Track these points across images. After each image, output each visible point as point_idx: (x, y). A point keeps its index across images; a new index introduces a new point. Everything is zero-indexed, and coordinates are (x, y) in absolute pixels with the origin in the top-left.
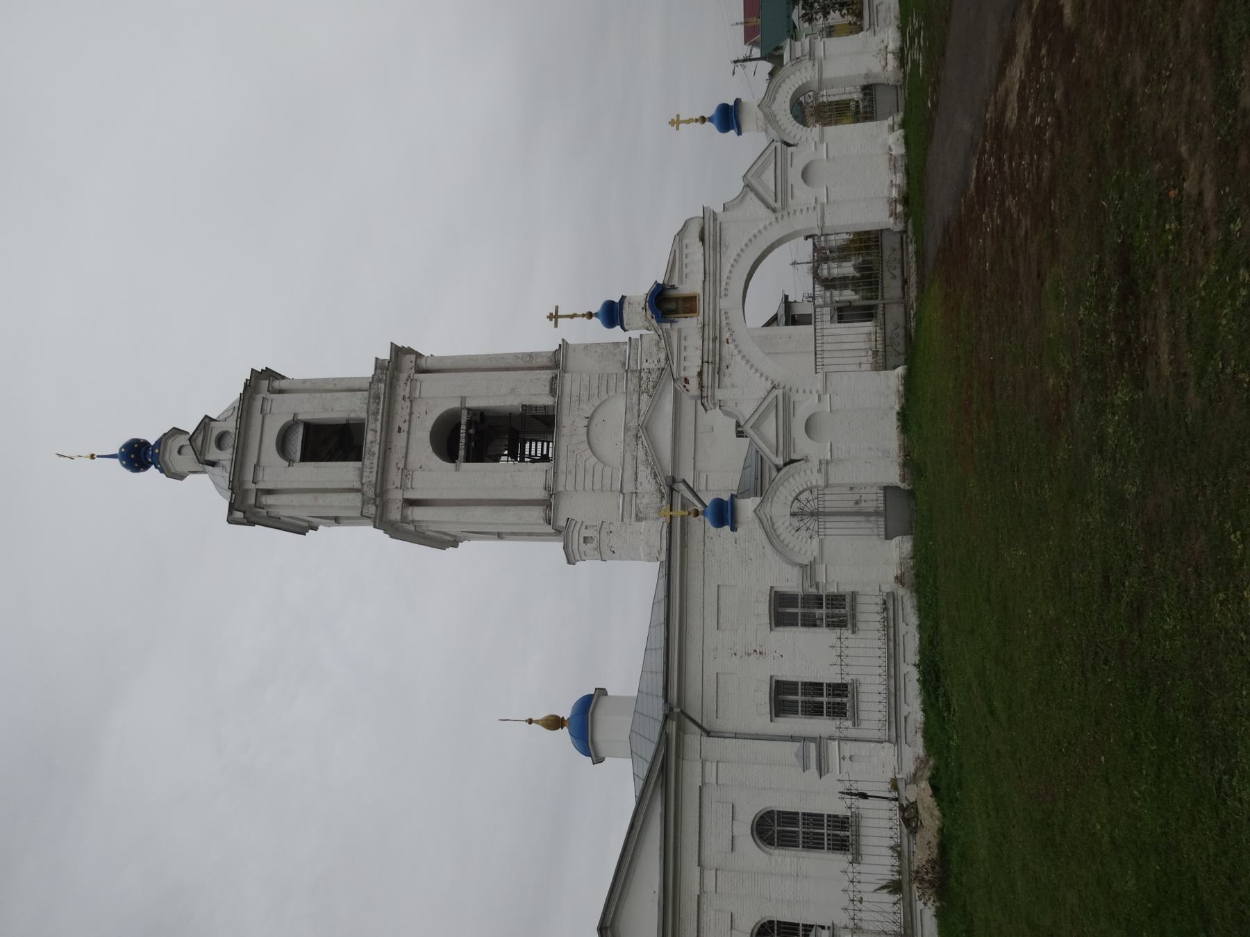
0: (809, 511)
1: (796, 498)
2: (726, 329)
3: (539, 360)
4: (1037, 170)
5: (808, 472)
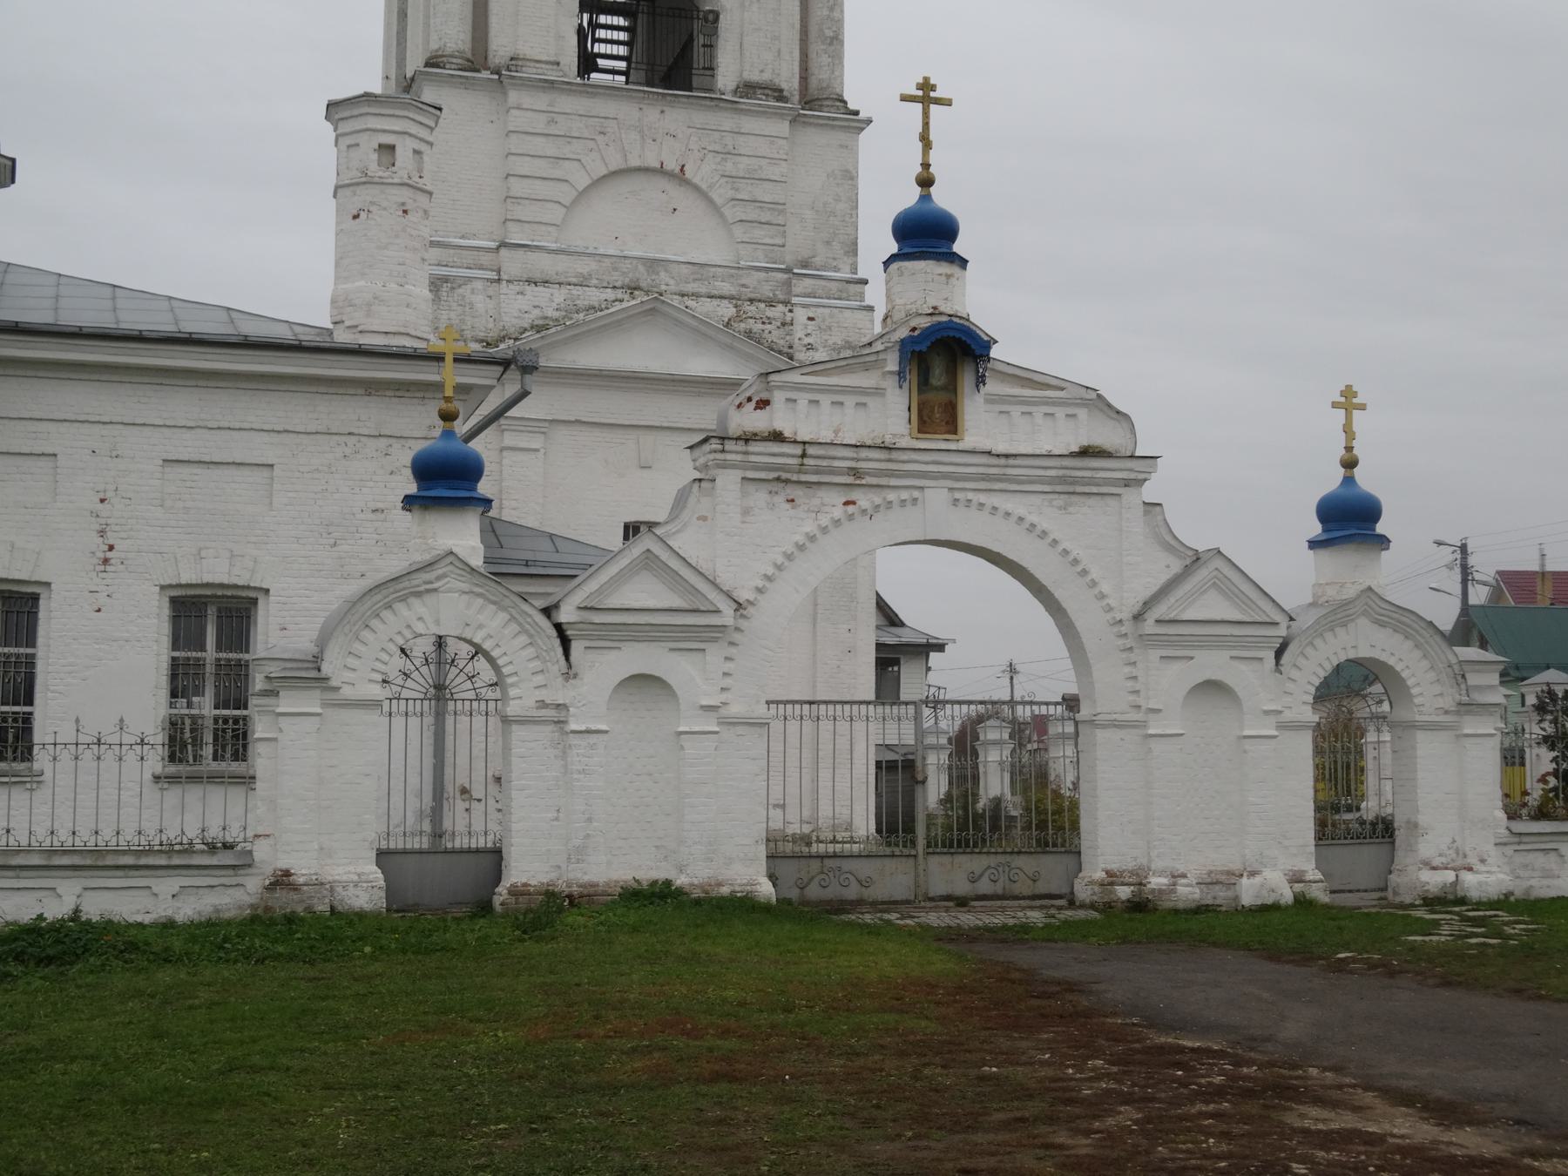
0: (447, 682)
1: (478, 650)
2: (878, 500)
3: (825, 59)
4: (1193, 1169)
5: (539, 679)
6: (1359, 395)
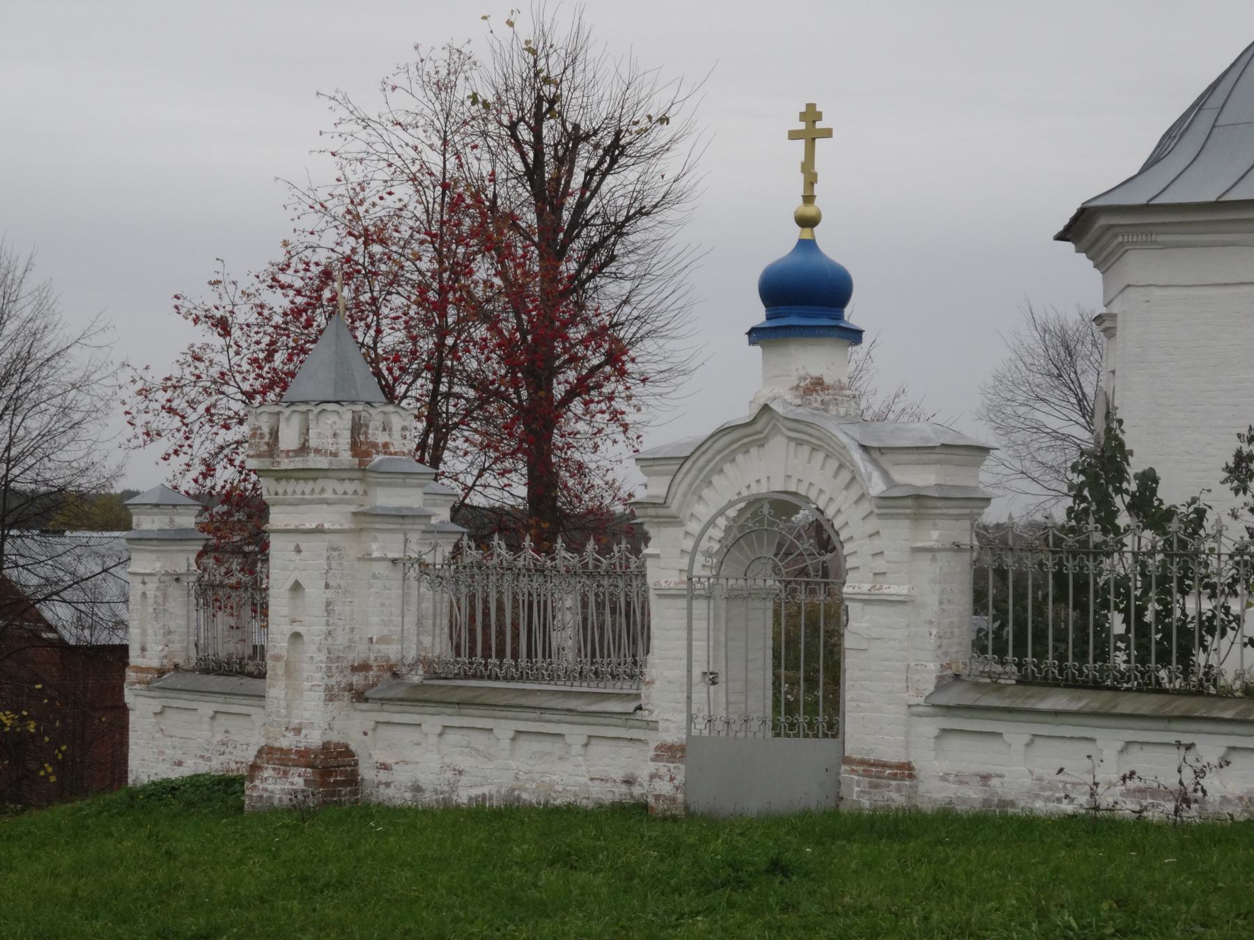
6: (824, 117)
